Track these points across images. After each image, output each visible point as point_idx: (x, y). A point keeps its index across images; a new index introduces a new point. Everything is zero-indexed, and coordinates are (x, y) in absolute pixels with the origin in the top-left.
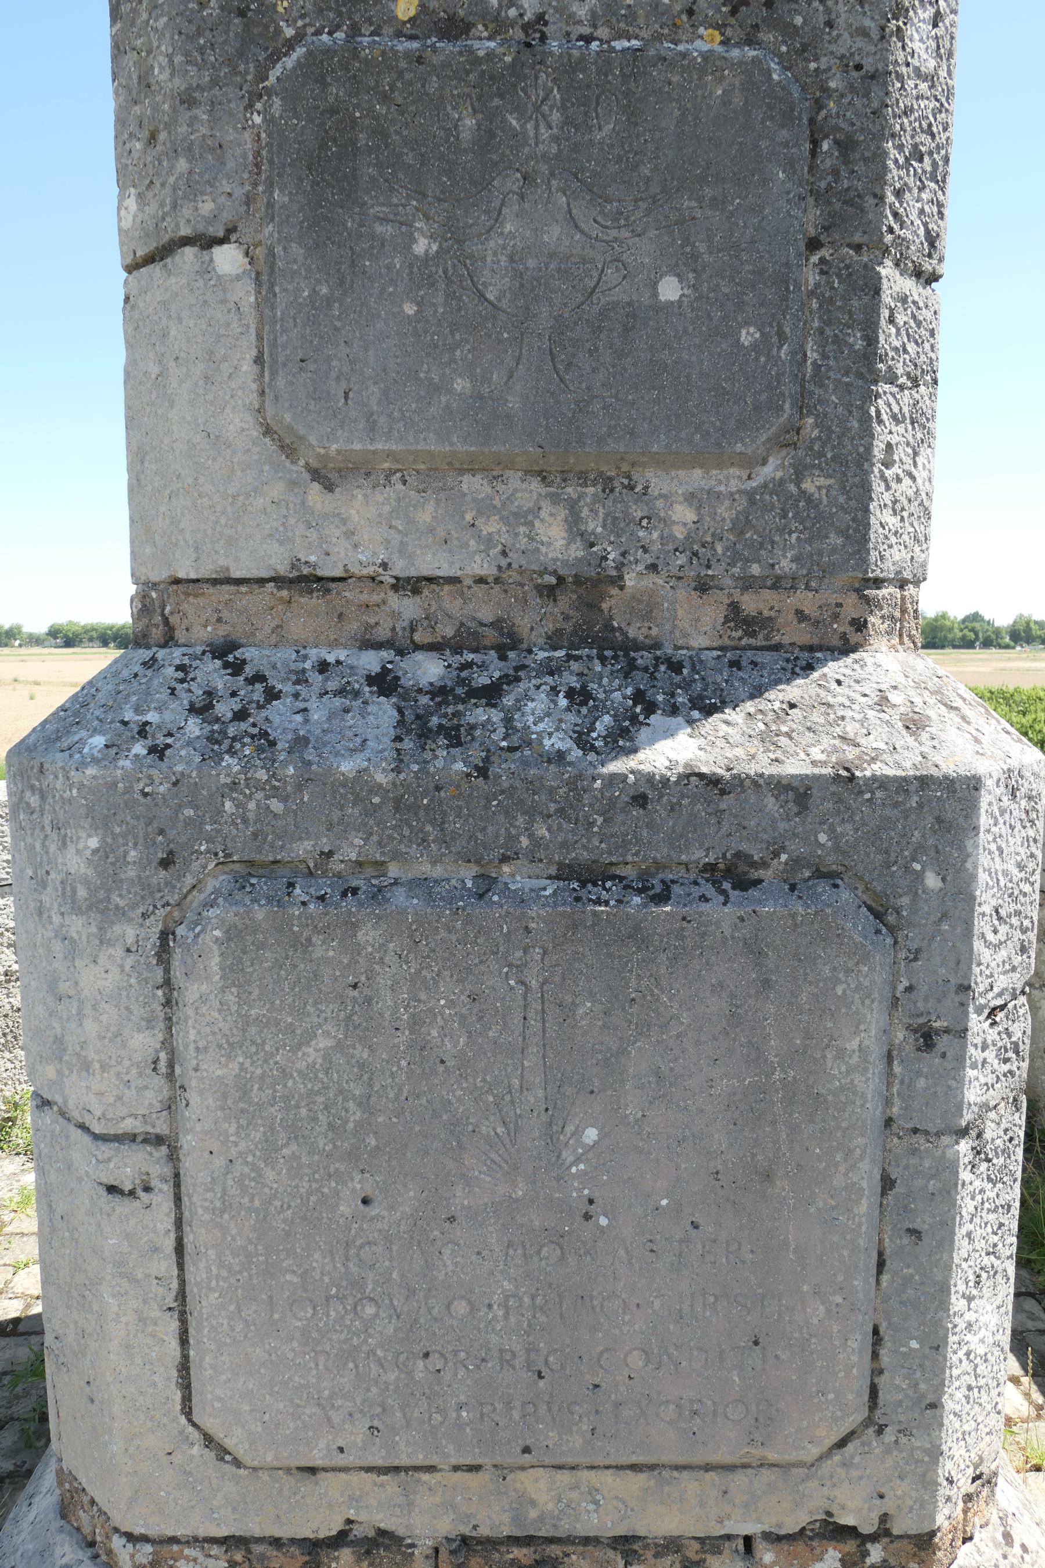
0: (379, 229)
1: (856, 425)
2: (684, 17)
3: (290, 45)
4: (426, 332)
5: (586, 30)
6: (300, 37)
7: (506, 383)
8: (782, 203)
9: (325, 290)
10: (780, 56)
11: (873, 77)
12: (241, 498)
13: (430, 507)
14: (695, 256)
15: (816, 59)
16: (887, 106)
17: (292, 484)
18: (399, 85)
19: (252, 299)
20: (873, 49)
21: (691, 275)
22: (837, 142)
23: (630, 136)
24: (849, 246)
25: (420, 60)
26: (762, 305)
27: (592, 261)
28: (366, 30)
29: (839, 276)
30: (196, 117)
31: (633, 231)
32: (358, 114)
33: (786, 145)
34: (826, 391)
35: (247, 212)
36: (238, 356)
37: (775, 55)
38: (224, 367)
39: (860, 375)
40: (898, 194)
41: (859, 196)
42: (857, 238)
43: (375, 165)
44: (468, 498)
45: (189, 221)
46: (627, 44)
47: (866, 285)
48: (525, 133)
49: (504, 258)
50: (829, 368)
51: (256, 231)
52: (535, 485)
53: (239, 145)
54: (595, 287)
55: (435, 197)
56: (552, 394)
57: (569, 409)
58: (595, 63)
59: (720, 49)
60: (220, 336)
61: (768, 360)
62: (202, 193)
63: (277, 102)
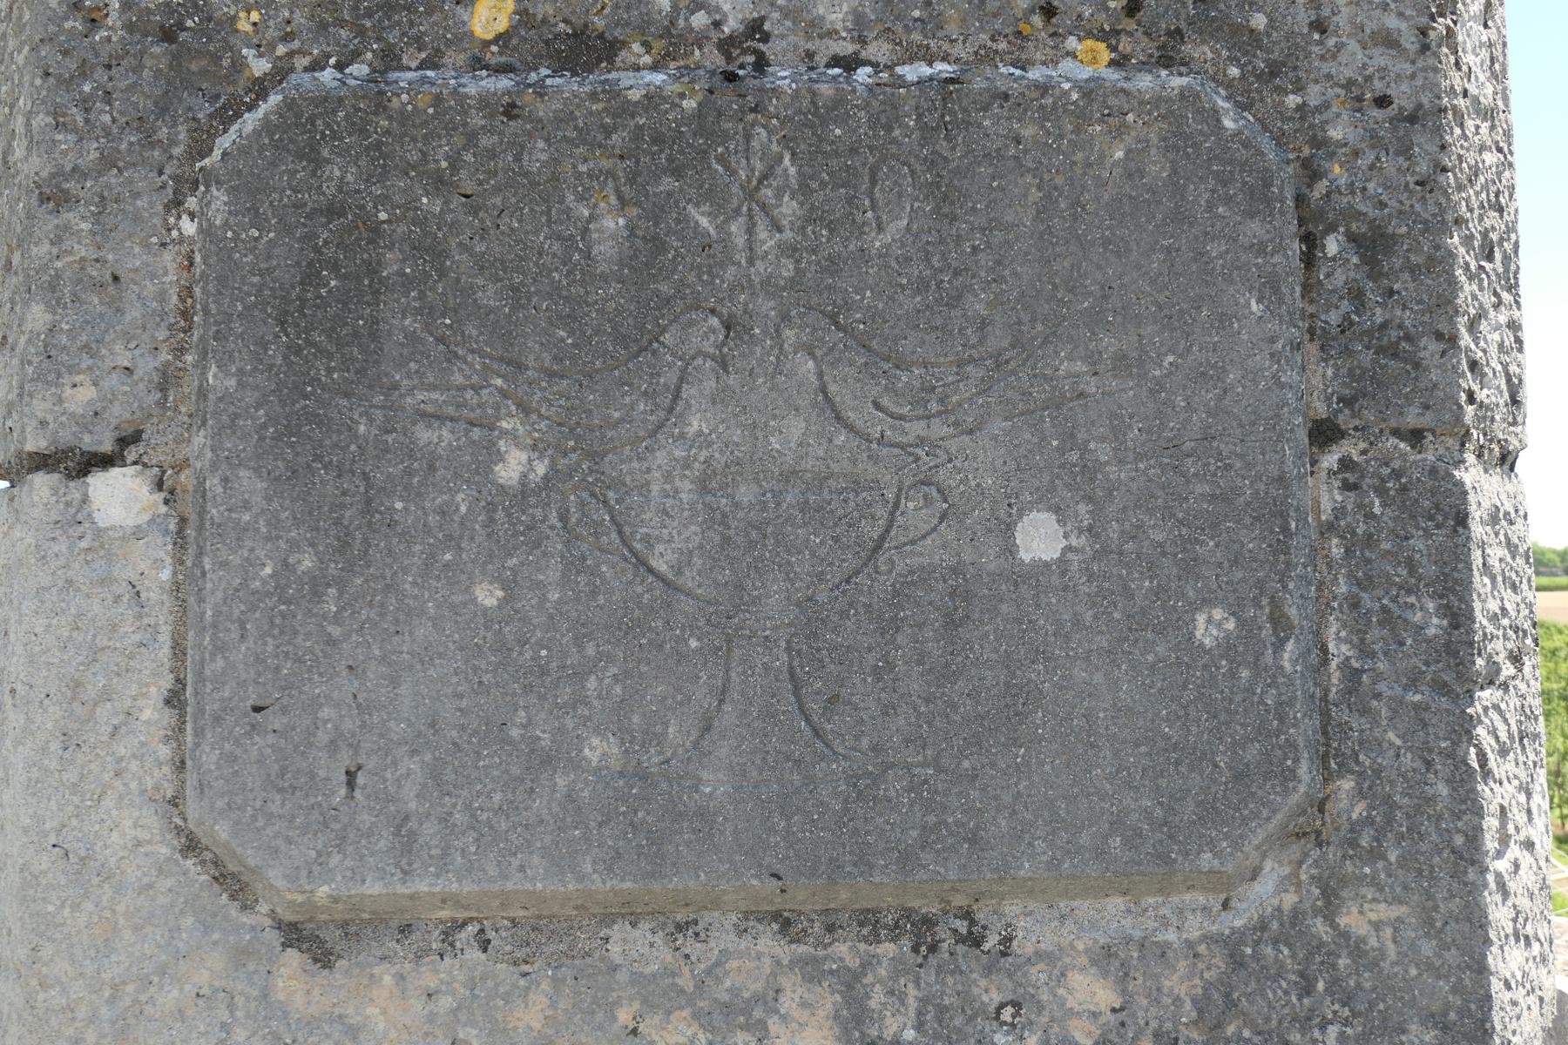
0: (424, 435)
1: (1443, 790)
2: (1037, 20)
3: (260, 89)
4: (523, 643)
5: (846, 48)
6: (281, 73)
7: (696, 744)
8: (1261, 360)
9: (307, 562)
10: (1229, 84)
11: (1413, 119)
12: (130, 988)
13: (539, 1000)
14: (1089, 470)
15: (1299, 89)
16: (1445, 170)
17: (241, 956)
18: (469, 158)
19: (166, 575)
20: (1408, 68)
21: (1083, 508)
22: (1352, 238)
23: (942, 241)
24: (1396, 433)
25: (511, 111)
26: (1235, 562)
27: (875, 485)
28: (411, 58)
29: (1381, 491)
30: (67, 227)
31: (956, 424)
32: (383, 216)
33: (1261, 250)
34: (1375, 722)
35: (162, 403)
36: (134, 690)
37: (1219, 83)
38: (103, 712)
39: (1441, 688)
40: (1472, 326)
41: (1408, 338)
42: (1412, 418)
43: (419, 311)
44: (622, 976)
45: (43, 423)
46: (926, 71)
47: (1437, 507)
48: (725, 239)
49: (687, 485)
50: (1378, 677)
51: (179, 441)
52: (768, 943)
53: (153, 276)
54: (882, 538)
55: (543, 370)
56: (798, 762)
57: (836, 794)
58: (866, 106)
59: (1113, 75)
60: (95, 654)
61: (1256, 675)
62: (73, 370)
63: (219, 197)
